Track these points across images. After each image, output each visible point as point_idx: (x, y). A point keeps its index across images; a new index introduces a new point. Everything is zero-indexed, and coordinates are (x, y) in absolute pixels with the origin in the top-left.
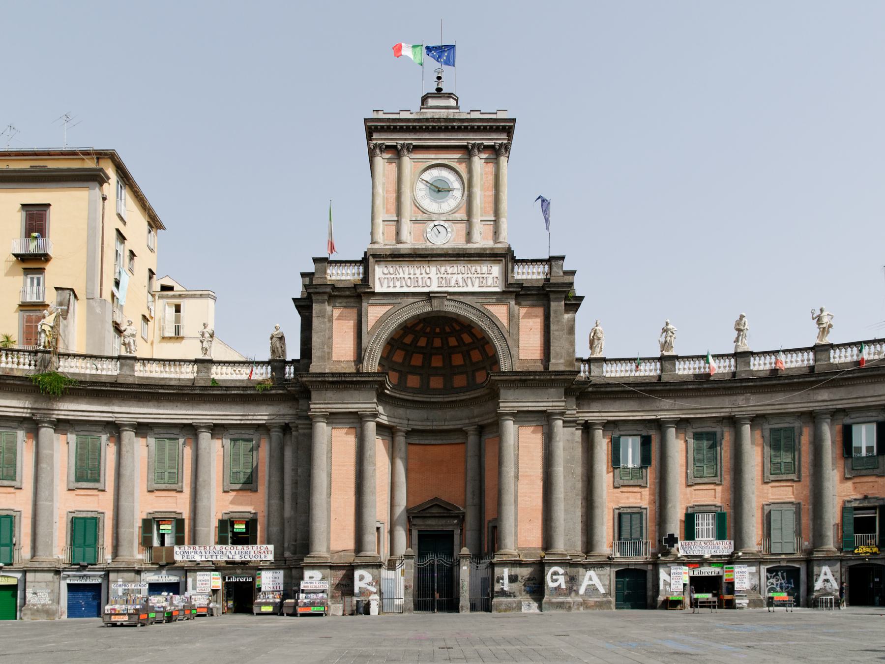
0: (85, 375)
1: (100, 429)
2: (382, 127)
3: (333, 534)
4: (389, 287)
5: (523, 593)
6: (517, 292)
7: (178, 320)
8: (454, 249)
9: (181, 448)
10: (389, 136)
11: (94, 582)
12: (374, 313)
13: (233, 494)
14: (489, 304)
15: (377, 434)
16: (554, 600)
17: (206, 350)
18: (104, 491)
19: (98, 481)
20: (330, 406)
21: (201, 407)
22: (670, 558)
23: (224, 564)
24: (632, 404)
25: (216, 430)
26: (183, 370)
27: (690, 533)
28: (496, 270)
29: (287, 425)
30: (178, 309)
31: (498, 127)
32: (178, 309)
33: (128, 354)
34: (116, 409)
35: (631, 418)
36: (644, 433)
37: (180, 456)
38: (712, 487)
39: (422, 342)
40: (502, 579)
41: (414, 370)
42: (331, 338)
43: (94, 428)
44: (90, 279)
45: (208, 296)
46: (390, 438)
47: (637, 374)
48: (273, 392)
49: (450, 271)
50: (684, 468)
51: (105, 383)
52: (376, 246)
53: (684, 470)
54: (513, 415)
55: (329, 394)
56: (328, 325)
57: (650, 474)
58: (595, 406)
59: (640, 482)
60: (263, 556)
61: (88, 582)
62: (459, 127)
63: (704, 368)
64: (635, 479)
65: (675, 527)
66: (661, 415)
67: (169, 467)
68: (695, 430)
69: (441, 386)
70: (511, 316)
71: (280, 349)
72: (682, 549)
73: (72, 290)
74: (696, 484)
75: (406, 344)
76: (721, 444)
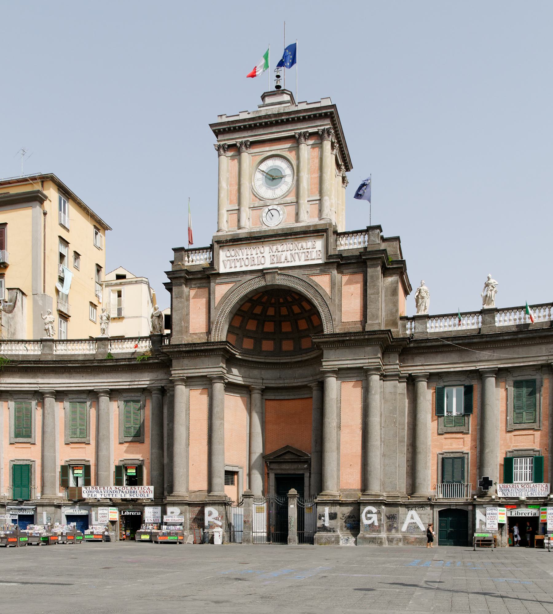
0: (18, 355)
1: (30, 396)
2: (224, 129)
3: (191, 479)
4: (231, 267)
5: (344, 529)
6: (338, 262)
7: (120, 303)
8: (283, 229)
9: (88, 409)
10: (235, 135)
11: (28, 514)
12: (220, 290)
13: (127, 445)
14: (313, 275)
15: (56, 401)
16: (367, 536)
17: (104, 330)
18: (34, 444)
19: (30, 437)
20: (186, 371)
21: (100, 376)
22: (486, 500)
23: (120, 501)
24: (454, 357)
25: (113, 394)
26: (124, 346)
27: (508, 477)
28: (319, 244)
29: (163, 387)
30: (119, 295)
31: (320, 115)
32: (119, 295)
33: (48, 338)
34: (40, 381)
35: (452, 370)
36: (467, 383)
37: (88, 415)
38: (531, 432)
39: (271, 312)
40: (324, 516)
41: (267, 336)
42: (188, 314)
43: (26, 396)
44: (35, 279)
45: (141, 282)
46: (248, 396)
47: (460, 328)
48: (151, 361)
49: (280, 249)
50: (505, 415)
51: (30, 361)
52: (220, 234)
53: (505, 417)
54: (334, 372)
55: (339, 353)
56: (186, 303)
57: (472, 421)
58: (419, 361)
59: (462, 429)
60: (146, 495)
61: (25, 514)
62: (288, 120)
63: (525, 319)
64: (455, 426)
65: (494, 471)
66: (481, 366)
67: (80, 425)
68: (515, 379)
69: (271, 349)
70: (333, 284)
71: (158, 326)
72: (499, 490)
73: (18, 289)
74: (516, 430)
75: (256, 314)
76: (540, 391)
